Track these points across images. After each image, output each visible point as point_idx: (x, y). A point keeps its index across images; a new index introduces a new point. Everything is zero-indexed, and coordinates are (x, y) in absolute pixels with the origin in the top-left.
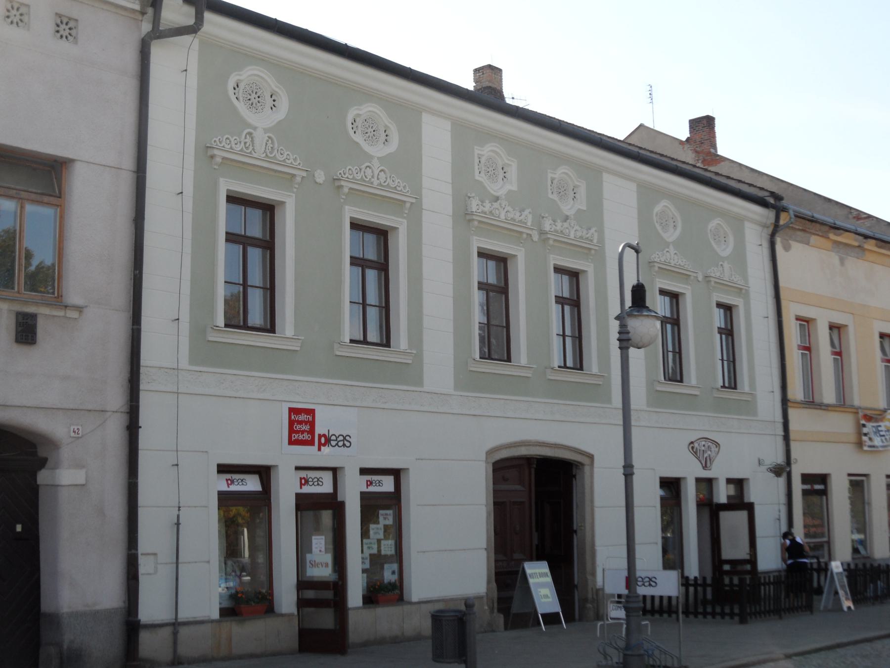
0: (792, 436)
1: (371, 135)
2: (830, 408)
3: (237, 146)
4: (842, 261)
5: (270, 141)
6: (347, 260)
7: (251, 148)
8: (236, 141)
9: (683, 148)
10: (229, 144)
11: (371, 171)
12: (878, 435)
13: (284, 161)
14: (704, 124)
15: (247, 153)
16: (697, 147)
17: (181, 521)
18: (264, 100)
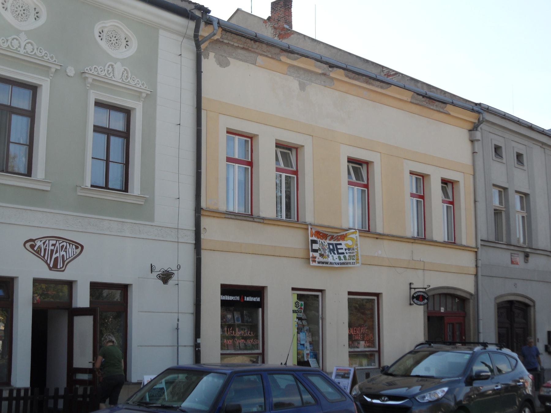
0: (204, 245)
1: (114, 42)
2: (265, 222)
3: (4, 44)
4: (302, 87)
5: (126, 72)
6: (91, 128)
7: (112, 75)
8: (101, 70)
9: (266, 26)
10: (96, 72)
11: (17, 42)
12: (336, 252)
13: (42, 57)
14: (281, 5)
15: (109, 77)
16: (275, 24)
17: (179, 327)
18: (12, 9)
